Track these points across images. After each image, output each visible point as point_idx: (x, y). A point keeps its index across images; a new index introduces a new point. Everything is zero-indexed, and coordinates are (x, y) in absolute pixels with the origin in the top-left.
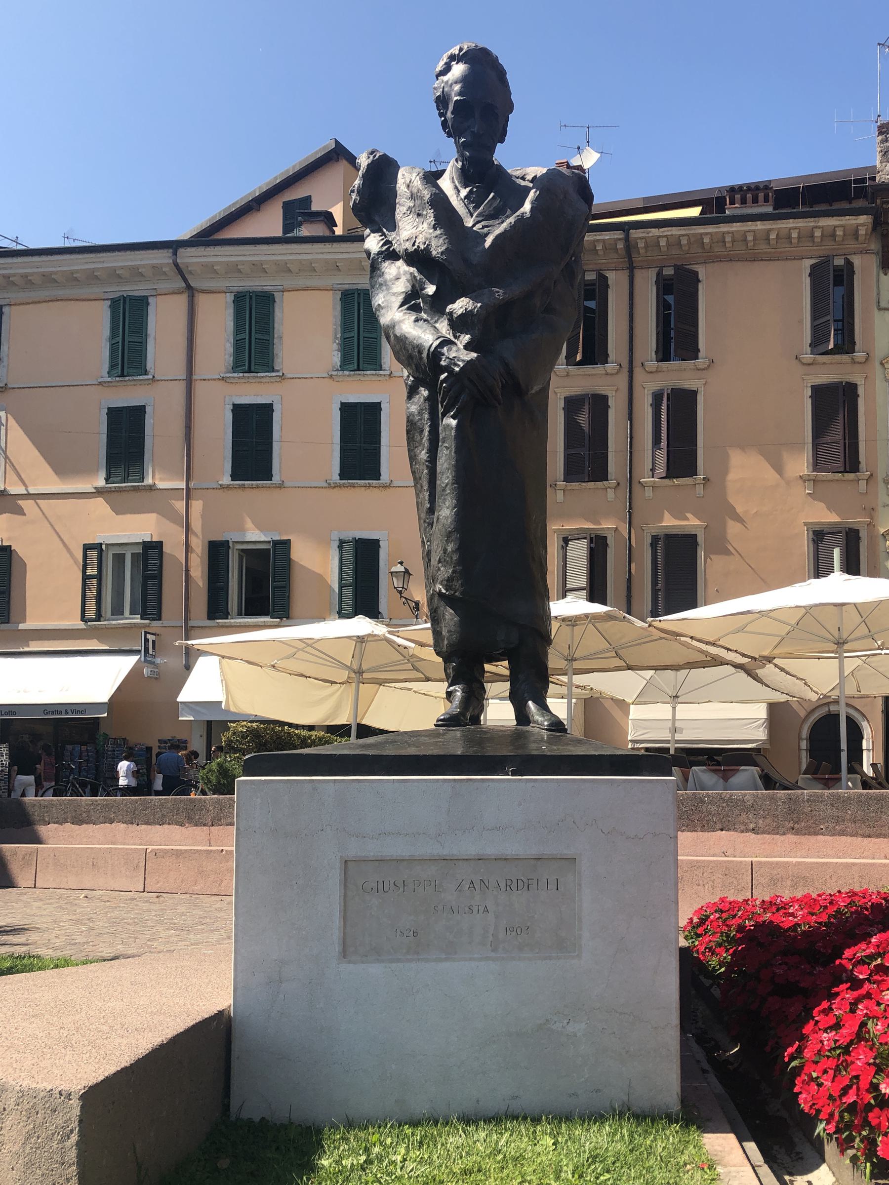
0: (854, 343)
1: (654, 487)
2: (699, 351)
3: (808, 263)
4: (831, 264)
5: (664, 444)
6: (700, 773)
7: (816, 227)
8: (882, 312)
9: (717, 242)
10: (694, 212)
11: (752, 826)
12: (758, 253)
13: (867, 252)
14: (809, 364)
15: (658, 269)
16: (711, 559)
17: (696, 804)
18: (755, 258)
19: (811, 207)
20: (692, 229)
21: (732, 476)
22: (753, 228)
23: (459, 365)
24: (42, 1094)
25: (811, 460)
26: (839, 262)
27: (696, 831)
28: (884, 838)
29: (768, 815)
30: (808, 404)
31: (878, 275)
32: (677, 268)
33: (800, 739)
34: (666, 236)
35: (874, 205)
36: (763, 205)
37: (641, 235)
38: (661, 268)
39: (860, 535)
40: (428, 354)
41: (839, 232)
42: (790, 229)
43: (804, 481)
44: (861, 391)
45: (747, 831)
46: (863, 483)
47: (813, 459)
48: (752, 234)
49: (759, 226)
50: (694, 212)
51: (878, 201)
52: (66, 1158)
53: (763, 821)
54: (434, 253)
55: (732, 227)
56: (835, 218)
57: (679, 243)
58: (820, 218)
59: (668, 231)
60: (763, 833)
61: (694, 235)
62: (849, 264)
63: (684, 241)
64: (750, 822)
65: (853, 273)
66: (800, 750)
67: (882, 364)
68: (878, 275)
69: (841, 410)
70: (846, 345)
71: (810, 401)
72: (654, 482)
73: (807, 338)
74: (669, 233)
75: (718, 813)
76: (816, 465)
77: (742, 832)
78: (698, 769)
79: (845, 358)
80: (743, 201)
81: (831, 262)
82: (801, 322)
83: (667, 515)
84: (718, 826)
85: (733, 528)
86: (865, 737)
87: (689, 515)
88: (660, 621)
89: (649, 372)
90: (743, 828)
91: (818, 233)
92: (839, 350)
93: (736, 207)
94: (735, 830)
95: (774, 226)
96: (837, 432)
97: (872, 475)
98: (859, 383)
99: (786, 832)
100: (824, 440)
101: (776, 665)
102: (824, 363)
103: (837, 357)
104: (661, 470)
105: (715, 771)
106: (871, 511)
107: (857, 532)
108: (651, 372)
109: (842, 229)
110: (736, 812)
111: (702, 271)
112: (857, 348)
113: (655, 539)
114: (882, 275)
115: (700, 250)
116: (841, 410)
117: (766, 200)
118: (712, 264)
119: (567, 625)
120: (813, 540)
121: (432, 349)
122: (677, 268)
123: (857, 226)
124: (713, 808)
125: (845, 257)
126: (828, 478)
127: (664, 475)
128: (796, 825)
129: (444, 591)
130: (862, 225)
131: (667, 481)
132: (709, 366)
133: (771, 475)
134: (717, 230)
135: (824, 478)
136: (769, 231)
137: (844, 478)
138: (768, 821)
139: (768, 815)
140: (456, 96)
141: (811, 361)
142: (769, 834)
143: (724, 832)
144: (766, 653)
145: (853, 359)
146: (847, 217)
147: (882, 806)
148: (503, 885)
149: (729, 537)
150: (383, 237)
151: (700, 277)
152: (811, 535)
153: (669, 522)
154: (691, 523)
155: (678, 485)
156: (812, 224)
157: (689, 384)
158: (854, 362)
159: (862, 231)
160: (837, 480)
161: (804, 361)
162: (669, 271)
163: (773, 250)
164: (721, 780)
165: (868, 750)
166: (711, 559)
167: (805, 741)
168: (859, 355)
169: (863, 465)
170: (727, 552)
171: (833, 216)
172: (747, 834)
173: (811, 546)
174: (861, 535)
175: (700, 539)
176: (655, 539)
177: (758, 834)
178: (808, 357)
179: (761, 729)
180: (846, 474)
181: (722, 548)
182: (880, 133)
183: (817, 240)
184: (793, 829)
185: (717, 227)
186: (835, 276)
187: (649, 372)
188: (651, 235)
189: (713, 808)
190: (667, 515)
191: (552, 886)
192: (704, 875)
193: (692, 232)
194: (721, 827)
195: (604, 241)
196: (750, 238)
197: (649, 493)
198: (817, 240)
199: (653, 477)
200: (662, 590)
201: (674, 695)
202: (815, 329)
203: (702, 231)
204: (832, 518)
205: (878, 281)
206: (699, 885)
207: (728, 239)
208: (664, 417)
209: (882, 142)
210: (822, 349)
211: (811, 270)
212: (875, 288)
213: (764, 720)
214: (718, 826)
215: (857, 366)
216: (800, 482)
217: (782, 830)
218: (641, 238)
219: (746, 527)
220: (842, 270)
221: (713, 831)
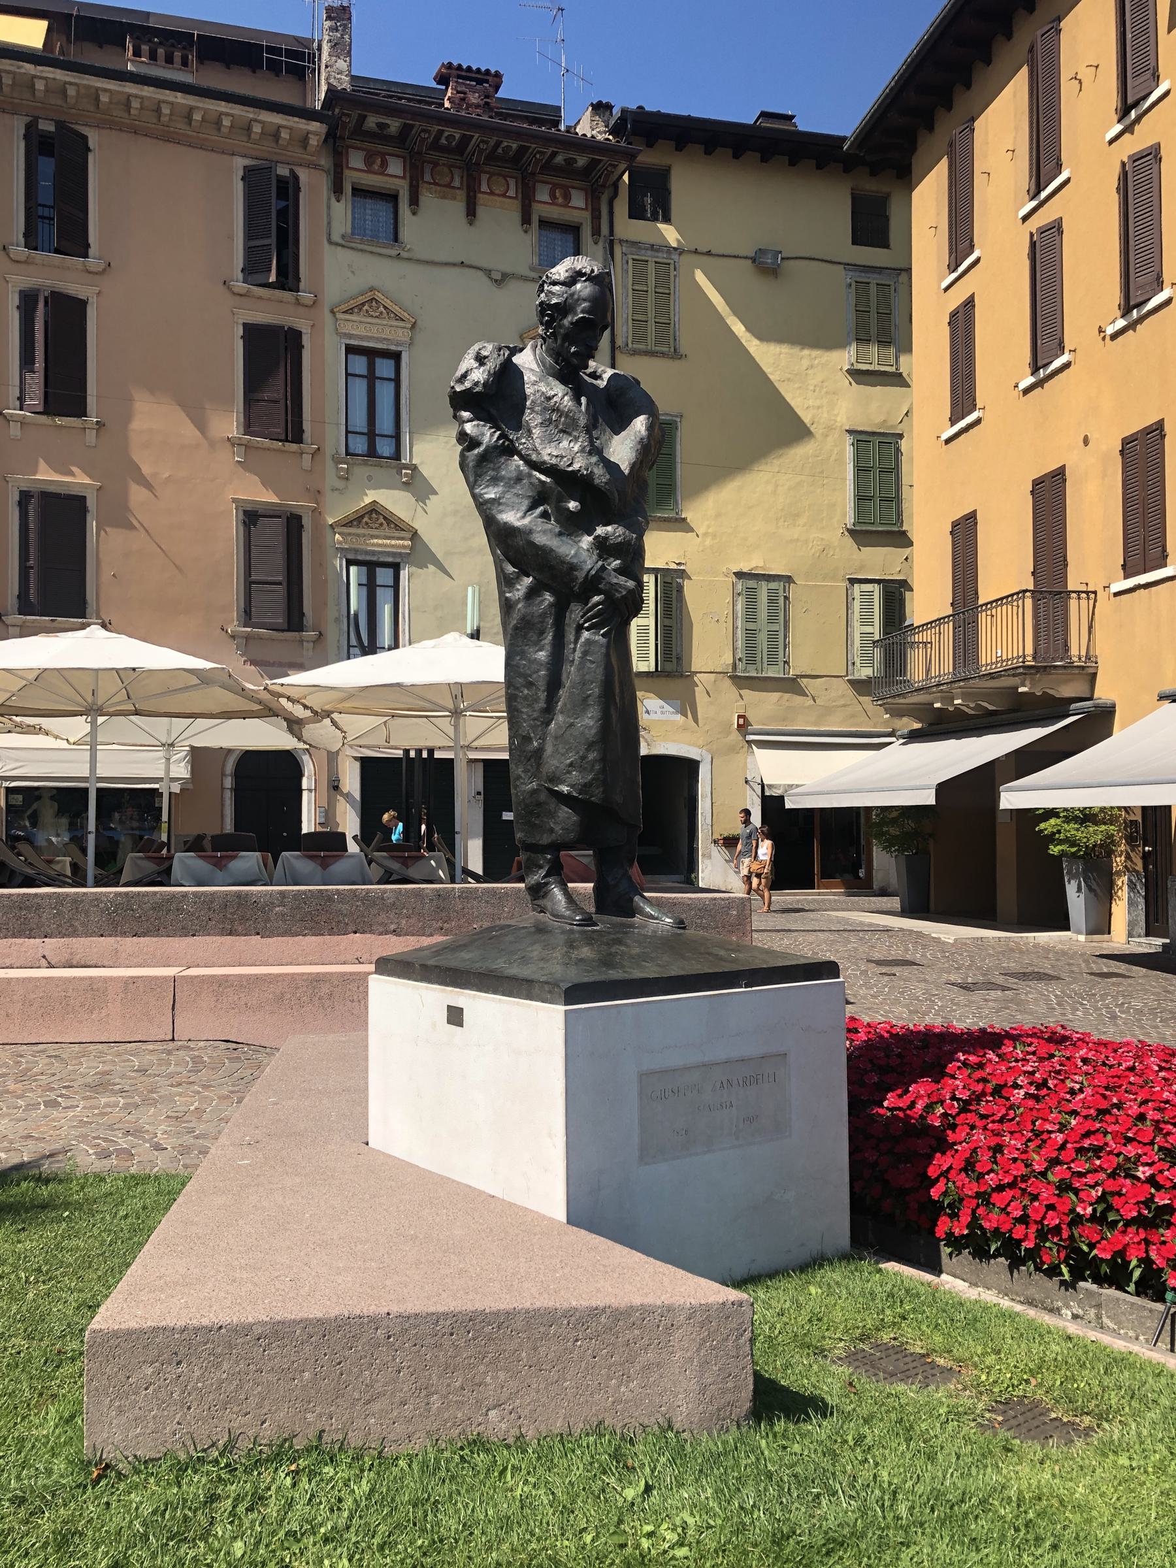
0: (298, 280)
1: (23, 423)
2: (88, 246)
3: (240, 163)
4: (273, 173)
5: (39, 365)
6: (293, 860)
7: (256, 120)
8: (333, 247)
11: (393, 927)
12: (174, 132)
13: (316, 167)
14: (241, 295)
15: (30, 118)
16: (106, 532)
18: (168, 137)
20: (84, 79)
21: (137, 425)
22: (171, 99)
23: (621, 592)
24: (715, 1307)
25: (242, 420)
26: (283, 171)
27: (322, 935)
30: (239, 346)
31: (329, 199)
32: (60, 125)
33: (223, 775)
34: (45, 78)
35: (330, 113)
36: (180, 69)
37: (8, 68)
38: (36, 120)
39: (303, 523)
40: (587, 575)
41: (285, 135)
42: (221, 114)
43: (233, 445)
44: (306, 341)
46: (307, 458)
47: (245, 418)
51: (337, 111)
52: (741, 1353)
54: (597, 481)
55: (142, 90)
56: (281, 115)
57: (64, 92)
58: (262, 111)
59: (49, 72)
61: (88, 87)
62: (296, 178)
63: (71, 92)
65: (298, 189)
66: (223, 789)
67: (332, 312)
68: (329, 199)
69: (282, 364)
70: (288, 279)
71: (241, 342)
72: (24, 417)
73: (239, 261)
74: (51, 76)
75: (351, 913)
76: (249, 426)
77: (381, 934)
78: (291, 855)
79: (287, 295)
80: (153, 57)
81: (273, 169)
82: (231, 237)
83: (42, 464)
84: (351, 927)
85: (137, 494)
86: (306, 774)
87: (74, 469)
88: (282, 685)
89: (14, 261)
91: (257, 129)
92: (281, 285)
93: (142, 62)
94: (372, 932)
95: (200, 105)
96: (276, 389)
97: (319, 449)
98: (304, 331)
100: (259, 396)
101: (334, 723)
102: (260, 298)
103: (278, 293)
104: (35, 400)
105: (311, 857)
106: (317, 494)
107: (299, 518)
108: (18, 262)
110: (374, 911)
111: (94, 138)
112: (302, 285)
113: (25, 498)
114: (333, 200)
115: (92, 108)
116: (282, 364)
118: (109, 131)
120: (244, 522)
121: (593, 572)
122: (60, 125)
123: (308, 133)
124: (345, 908)
125: (290, 167)
126: (265, 446)
127: (41, 409)
128: (445, 925)
129: (575, 794)
130: (316, 134)
131: (43, 419)
132: (104, 270)
133: (189, 431)
134: (120, 89)
135: (259, 445)
136: (191, 109)
137: (283, 448)
138: (412, 921)
140: (582, 312)
141: (243, 292)
142: (413, 935)
144: (327, 707)
145: (297, 299)
146: (296, 119)
148: (741, 1082)
149: (132, 504)
150: (929, 645)
151: (91, 144)
152: (241, 516)
153: (46, 475)
154: (78, 480)
155: (60, 426)
156: (251, 116)
157: (75, 288)
158: (298, 303)
159: (314, 141)
160: (274, 450)
161: (236, 290)
162: (47, 126)
163: (195, 134)
164: (320, 868)
165: (310, 790)
166: (106, 532)
167: (229, 779)
168: (305, 296)
169: (307, 436)
170: (132, 527)
171: (278, 113)
172: (387, 936)
173: (241, 528)
174: (304, 522)
175: (91, 503)
176: (25, 498)
177: (400, 936)
178: (240, 286)
179: (183, 764)
180: (287, 444)
181: (122, 519)
182: (329, 18)
184: (442, 929)
185: (120, 85)
186: (278, 187)
187: (14, 261)
188: (23, 71)
189: (345, 908)
190: (42, 464)
191: (771, 1079)
193: (85, 82)
194: (354, 929)
196: (166, 110)
197: (15, 430)
199: (21, 409)
200: (36, 568)
201: (170, 742)
202: (249, 251)
203: (99, 85)
204: (268, 497)
205: (329, 207)
206: (353, 1001)
207: (135, 104)
208: (39, 326)
209: (331, 29)
210: (260, 278)
211: (245, 173)
212: (325, 216)
213: (186, 753)
214: (351, 927)
215: (302, 310)
216: (228, 444)
217: (428, 931)
218: (8, 72)
219: (156, 496)
220: (287, 183)
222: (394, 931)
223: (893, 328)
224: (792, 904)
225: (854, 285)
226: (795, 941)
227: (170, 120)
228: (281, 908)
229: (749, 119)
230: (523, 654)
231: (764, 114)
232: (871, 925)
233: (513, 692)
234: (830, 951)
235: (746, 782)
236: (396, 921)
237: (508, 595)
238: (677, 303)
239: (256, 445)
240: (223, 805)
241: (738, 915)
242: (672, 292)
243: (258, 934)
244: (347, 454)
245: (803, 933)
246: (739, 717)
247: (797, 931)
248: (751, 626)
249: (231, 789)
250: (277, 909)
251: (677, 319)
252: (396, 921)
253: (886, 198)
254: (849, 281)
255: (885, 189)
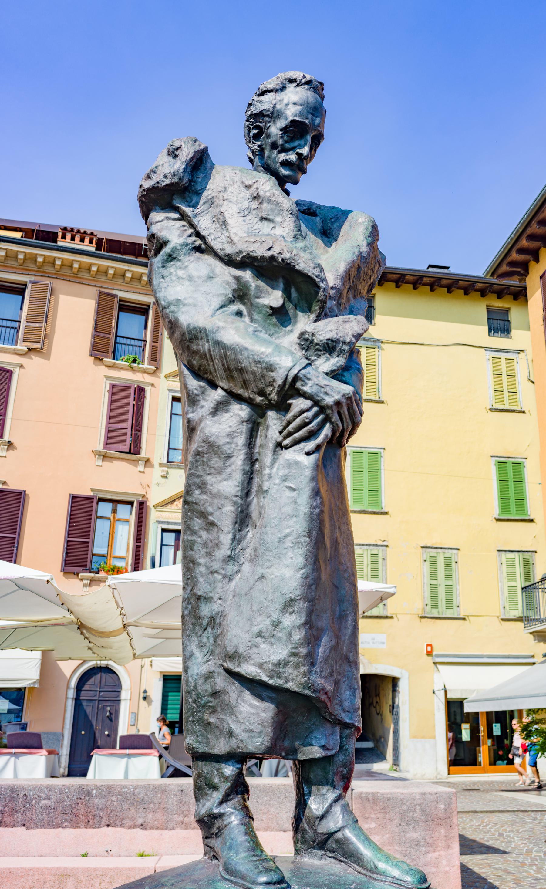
7: (129, 270)
9: (48, 263)
10: (17, 235)
11: (140, 821)
17: (83, 798)
19: (136, 258)
28: (271, 831)
29: (159, 808)
33: (68, 687)
42: (108, 267)
45: (134, 827)
48: (79, 263)
49: (85, 259)
50: (17, 235)
53: (153, 816)
60: (152, 828)
64: (139, 817)
66: (67, 698)
77: (130, 828)
90: (131, 823)
94: (122, 826)
99: (175, 826)
109: (79, 263)
117: (91, 242)
119: (541, 757)
126: (116, 456)
128: (186, 819)
135: (112, 456)
139: (159, 808)
141: (112, 365)
143: (110, 828)
147: (271, 798)
177: (146, 829)
183: (110, 276)
192: (102, 884)
194: (108, 823)
195: (133, 272)
198: (110, 276)
221: (98, 828)
222: (142, 825)
223: (517, 384)
224: (470, 786)
225: (491, 359)
226: (483, 822)
227: (78, 271)
228: (46, 801)
229: (423, 267)
230: (202, 487)
231: (430, 266)
232: (536, 805)
233: (190, 538)
234: (512, 831)
235: (434, 693)
236: (144, 815)
237: (190, 415)
238: (380, 370)
239: (109, 455)
240: (65, 711)
241: (445, 810)
242: (377, 364)
243: (24, 825)
244: (168, 462)
245: (488, 814)
246: (428, 645)
247: (482, 812)
248: (434, 582)
249: (73, 698)
250: (43, 802)
251: (380, 379)
252: (144, 815)
253: (508, 311)
254: (488, 357)
255: (506, 305)
